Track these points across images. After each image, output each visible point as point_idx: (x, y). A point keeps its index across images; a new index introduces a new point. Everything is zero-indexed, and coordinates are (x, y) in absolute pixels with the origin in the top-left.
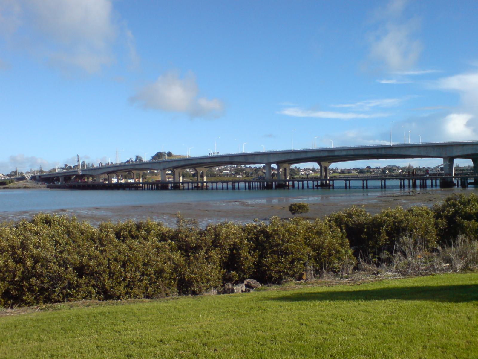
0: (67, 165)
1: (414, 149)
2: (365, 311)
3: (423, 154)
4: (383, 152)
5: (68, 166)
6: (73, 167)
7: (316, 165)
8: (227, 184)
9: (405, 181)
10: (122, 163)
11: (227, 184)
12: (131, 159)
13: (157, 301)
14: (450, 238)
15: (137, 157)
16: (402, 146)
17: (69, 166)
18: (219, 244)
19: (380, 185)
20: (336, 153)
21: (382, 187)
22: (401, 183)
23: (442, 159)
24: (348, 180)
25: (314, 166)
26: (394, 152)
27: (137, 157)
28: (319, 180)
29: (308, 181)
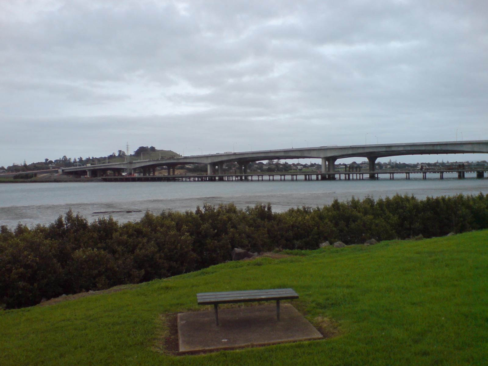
0: (48, 160)
1: (464, 146)
2: (174, 329)
3: (475, 150)
4: (439, 148)
5: (49, 161)
6: (54, 162)
7: (365, 159)
8: (252, 177)
9: (426, 174)
10: (191, 156)
11: (252, 177)
12: (114, 153)
13: (316, 323)
14: (180, 239)
15: (120, 151)
16: (354, 147)
17: (50, 161)
18: (356, 241)
19: (405, 177)
20: (394, 149)
21: (391, 179)
22: (407, 176)
23: (321, 159)
24: (294, 175)
25: (396, 160)
26: (444, 148)
27: (120, 151)
28: (217, 176)
29: (340, 174)
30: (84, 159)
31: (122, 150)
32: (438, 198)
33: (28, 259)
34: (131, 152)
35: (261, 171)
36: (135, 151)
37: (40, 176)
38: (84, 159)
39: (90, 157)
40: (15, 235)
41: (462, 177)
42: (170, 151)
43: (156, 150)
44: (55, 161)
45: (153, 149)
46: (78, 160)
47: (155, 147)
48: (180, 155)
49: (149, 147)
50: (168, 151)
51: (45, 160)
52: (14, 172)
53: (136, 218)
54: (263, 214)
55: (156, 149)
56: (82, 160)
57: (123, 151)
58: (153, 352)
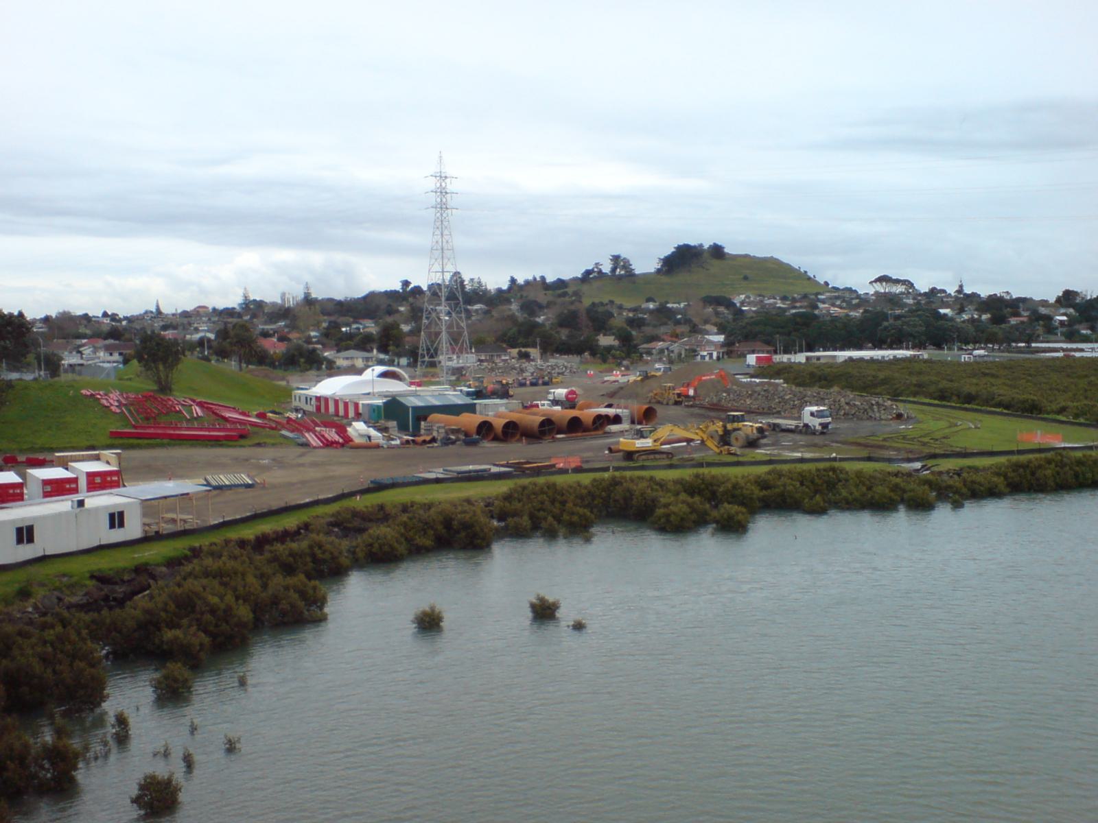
12: (597, 264)
15: (616, 259)
27: (616, 259)
30: (521, 281)
31: (623, 256)
33: (776, 393)
34: (646, 264)
36: (662, 257)
38: (521, 281)
39: (536, 276)
40: (1079, 315)
42: (772, 257)
43: (728, 254)
44: (430, 287)
45: (717, 251)
46: (538, 279)
47: (724, 245)
48: (802, 270)
49: (706, 246)
50: (765, 260)
51: (401, 284)
53: (869, 358)
54: (1049, 348)
55: (726, 250)
56: (634, 275)
57: (624, 259)
58: (315, 592)
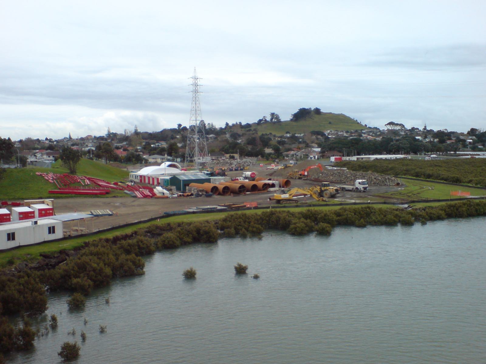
12: (264, 117)
15: (273, 114)
27: (273, 114)
30: (230, 124)
31: (276, 113)
32: (184, 273)
34: (286, 117)
35: (222, 169)
36: (293, 114)
37: (348, 201)
38: (230, 124)
39: (237, 122)
41: (182, 181)
42: (342, 114)
43: (322, 112)
44: (191, 127)
45: (317, 111)
46: (238, 123)
47: (320, 108)
48: (355, 120)
49: (313, 109)
50: (339, 115)
51: (177, 126)
52: (363, 155)
55: (321, 111)
56: (281, 122)
57: (276, 114)
